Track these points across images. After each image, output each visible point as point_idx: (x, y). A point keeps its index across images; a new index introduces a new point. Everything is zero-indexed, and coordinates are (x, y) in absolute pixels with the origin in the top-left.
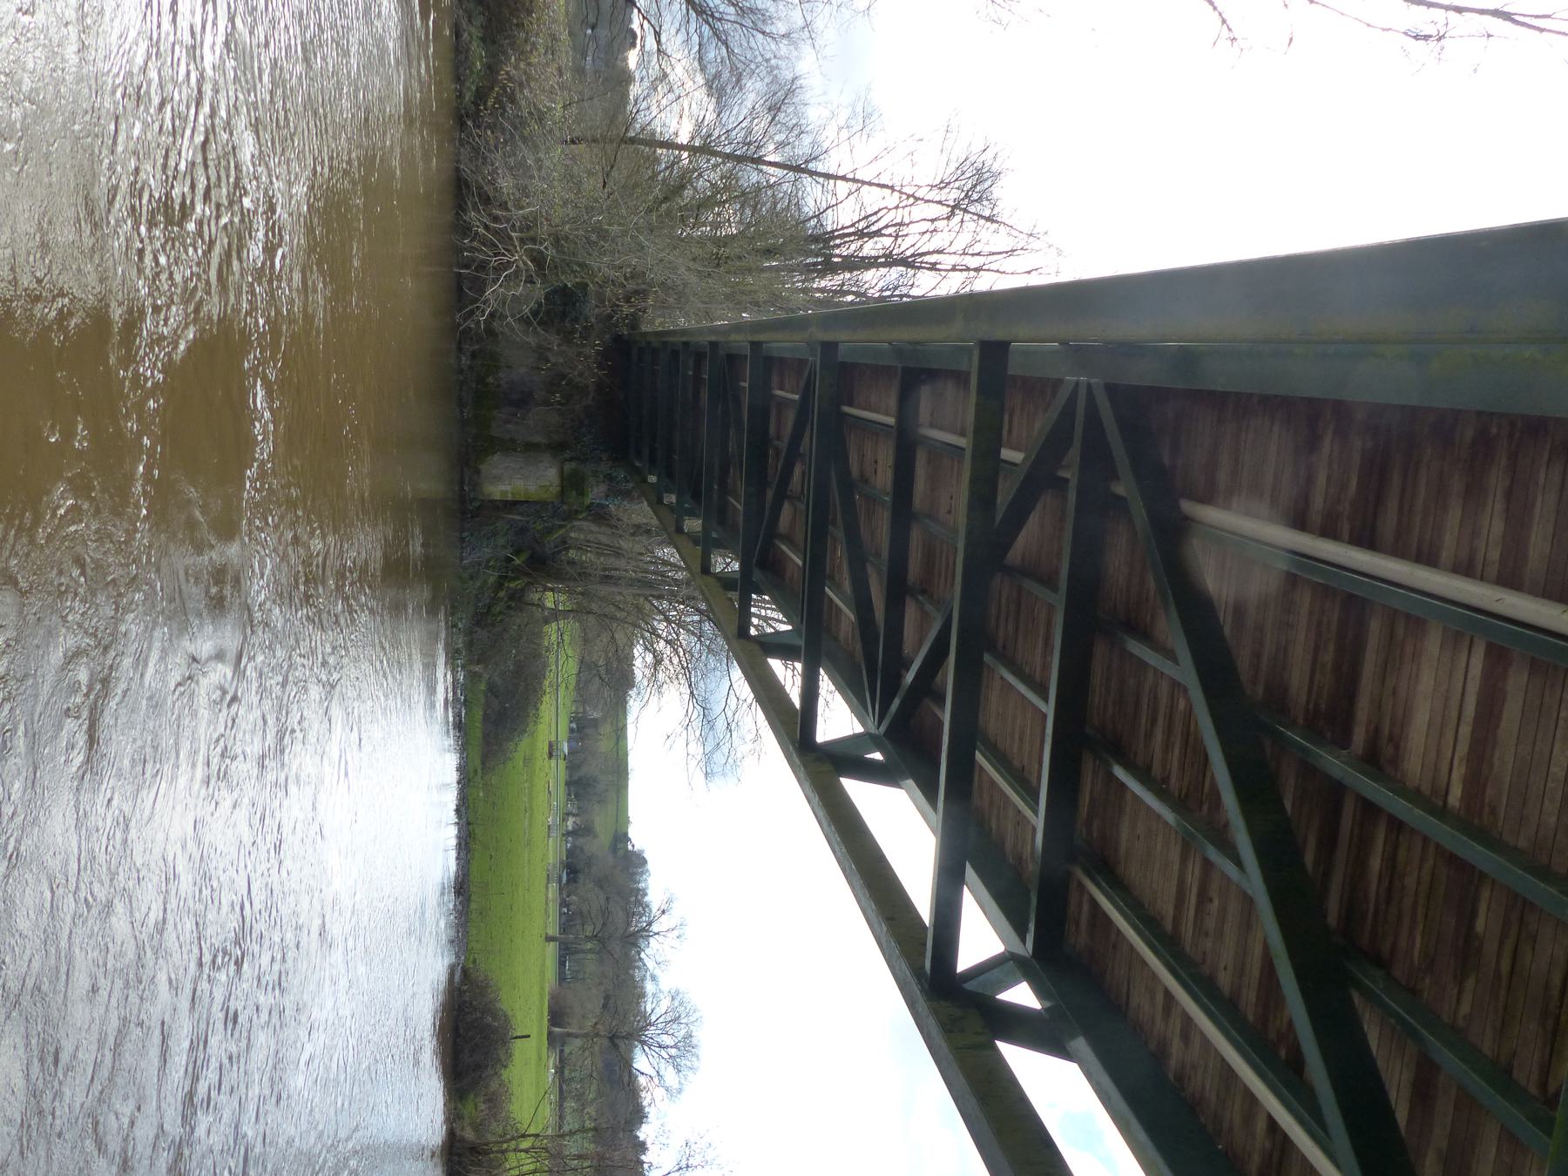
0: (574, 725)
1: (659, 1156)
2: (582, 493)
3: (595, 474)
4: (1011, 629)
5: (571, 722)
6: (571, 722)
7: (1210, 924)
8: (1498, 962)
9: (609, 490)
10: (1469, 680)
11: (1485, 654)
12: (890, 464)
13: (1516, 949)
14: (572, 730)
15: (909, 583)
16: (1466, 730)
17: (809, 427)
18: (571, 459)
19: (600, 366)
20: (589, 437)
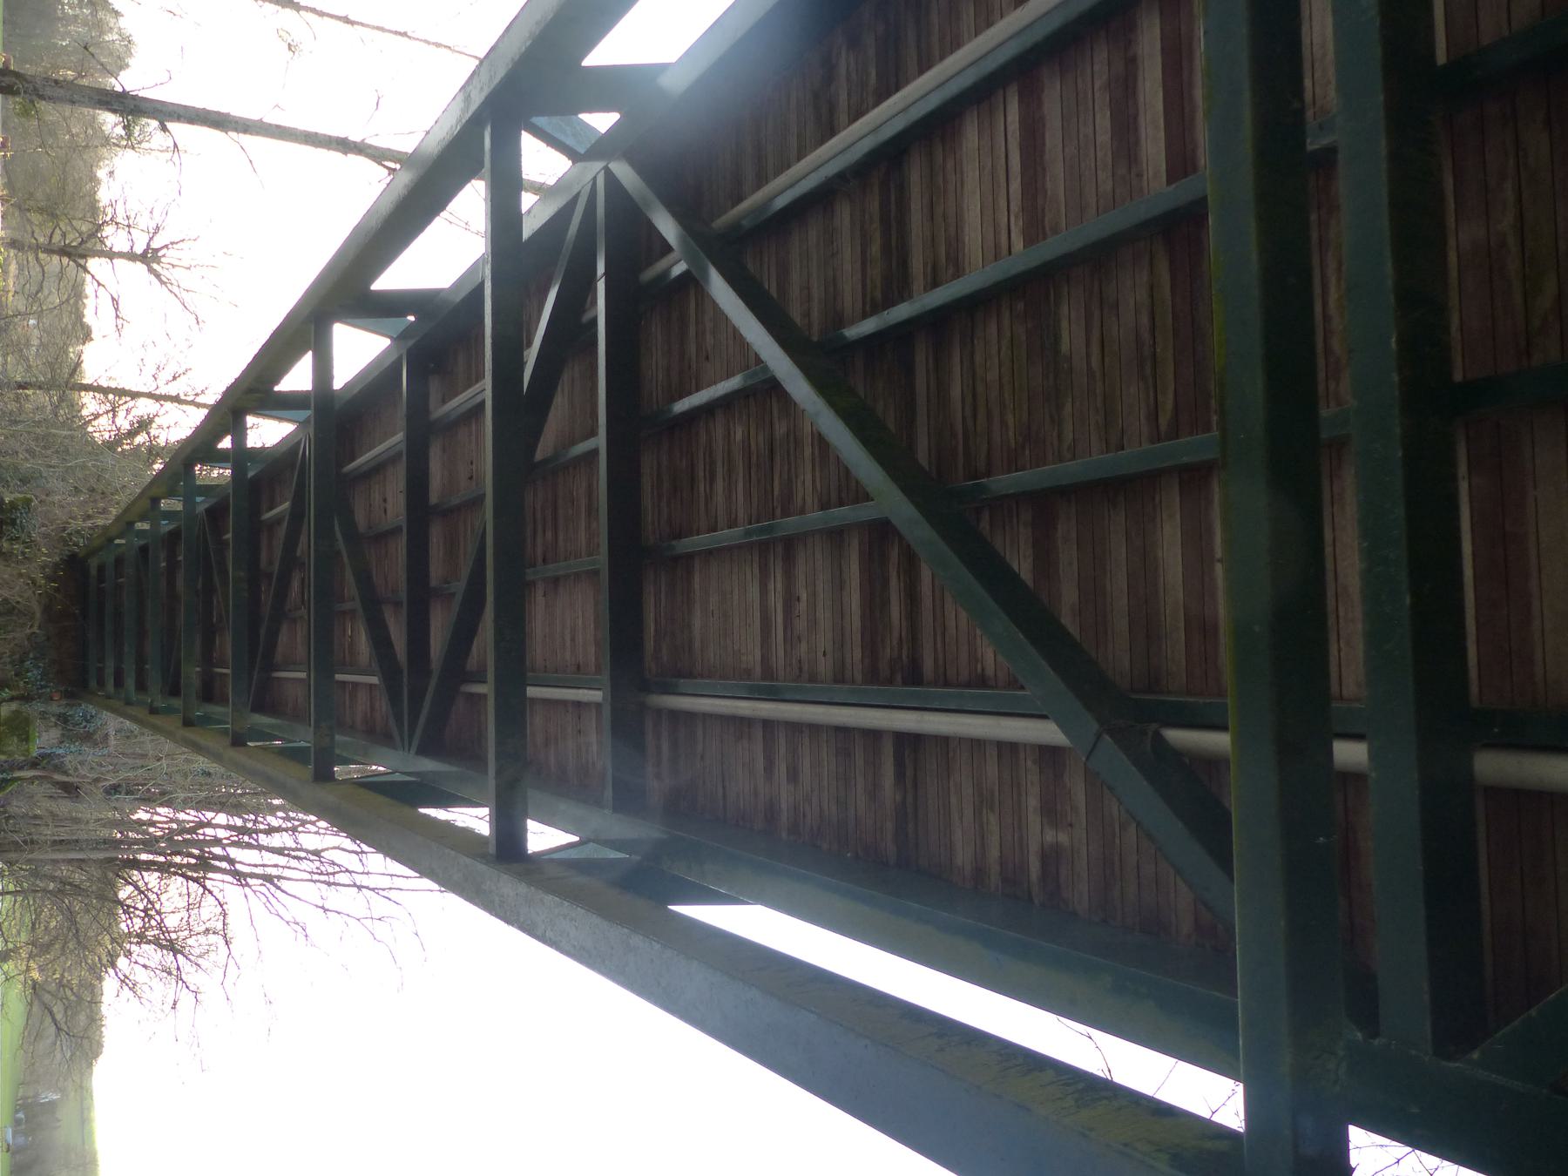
0: (21, 1115)
1: (84, 1166)
2: (26, 739)
3: (43, 716)
4: (549, 534)
5: (17, 1111)
6: (17, 1111)
7: (801, 625)
8: (1089, 363)
9: (63, 735)
10: (1009, 137)
11: (1019, 102)
12: (402, 489)
13: (855, 143)
14: (17, 1122)
15: (468, 667)
16: (1016, 186)
17: (306, 520)
18: (12, 699)
19: (49, 579)
20: (35, 672)
